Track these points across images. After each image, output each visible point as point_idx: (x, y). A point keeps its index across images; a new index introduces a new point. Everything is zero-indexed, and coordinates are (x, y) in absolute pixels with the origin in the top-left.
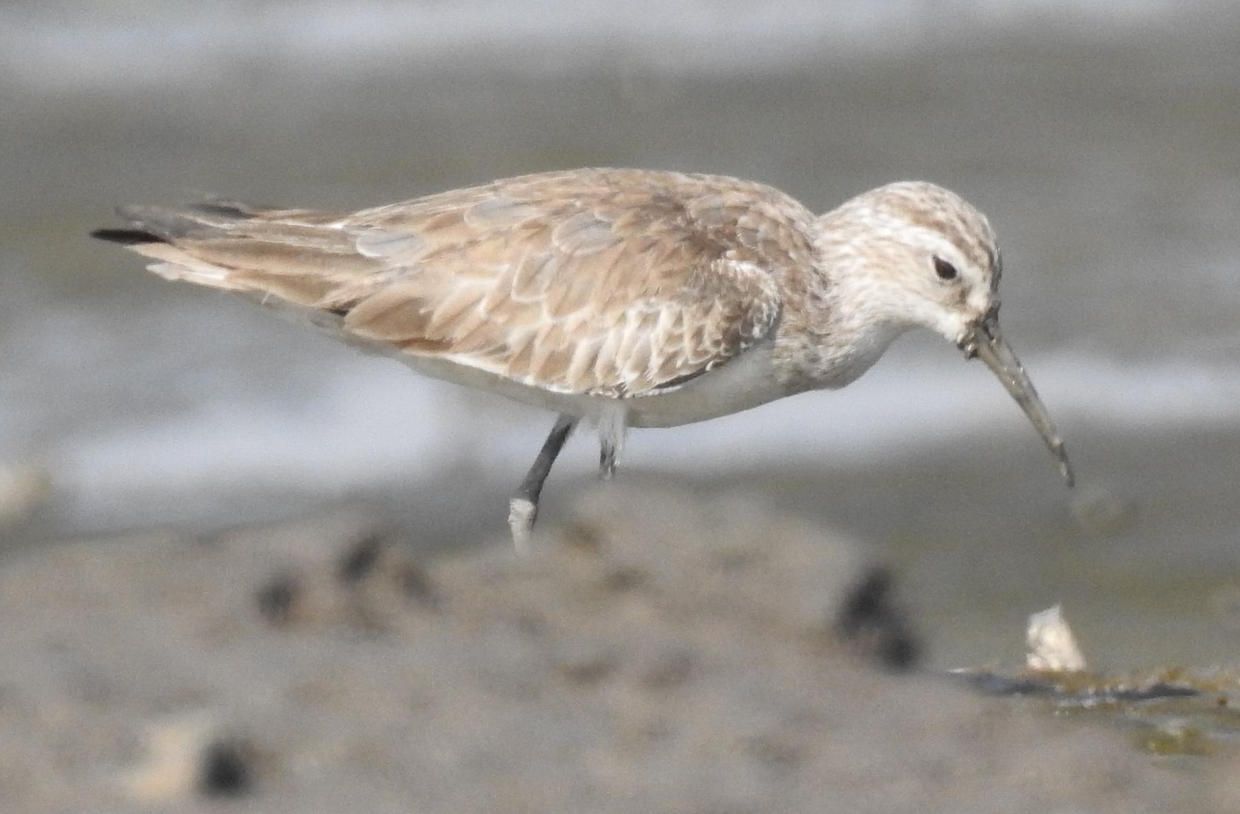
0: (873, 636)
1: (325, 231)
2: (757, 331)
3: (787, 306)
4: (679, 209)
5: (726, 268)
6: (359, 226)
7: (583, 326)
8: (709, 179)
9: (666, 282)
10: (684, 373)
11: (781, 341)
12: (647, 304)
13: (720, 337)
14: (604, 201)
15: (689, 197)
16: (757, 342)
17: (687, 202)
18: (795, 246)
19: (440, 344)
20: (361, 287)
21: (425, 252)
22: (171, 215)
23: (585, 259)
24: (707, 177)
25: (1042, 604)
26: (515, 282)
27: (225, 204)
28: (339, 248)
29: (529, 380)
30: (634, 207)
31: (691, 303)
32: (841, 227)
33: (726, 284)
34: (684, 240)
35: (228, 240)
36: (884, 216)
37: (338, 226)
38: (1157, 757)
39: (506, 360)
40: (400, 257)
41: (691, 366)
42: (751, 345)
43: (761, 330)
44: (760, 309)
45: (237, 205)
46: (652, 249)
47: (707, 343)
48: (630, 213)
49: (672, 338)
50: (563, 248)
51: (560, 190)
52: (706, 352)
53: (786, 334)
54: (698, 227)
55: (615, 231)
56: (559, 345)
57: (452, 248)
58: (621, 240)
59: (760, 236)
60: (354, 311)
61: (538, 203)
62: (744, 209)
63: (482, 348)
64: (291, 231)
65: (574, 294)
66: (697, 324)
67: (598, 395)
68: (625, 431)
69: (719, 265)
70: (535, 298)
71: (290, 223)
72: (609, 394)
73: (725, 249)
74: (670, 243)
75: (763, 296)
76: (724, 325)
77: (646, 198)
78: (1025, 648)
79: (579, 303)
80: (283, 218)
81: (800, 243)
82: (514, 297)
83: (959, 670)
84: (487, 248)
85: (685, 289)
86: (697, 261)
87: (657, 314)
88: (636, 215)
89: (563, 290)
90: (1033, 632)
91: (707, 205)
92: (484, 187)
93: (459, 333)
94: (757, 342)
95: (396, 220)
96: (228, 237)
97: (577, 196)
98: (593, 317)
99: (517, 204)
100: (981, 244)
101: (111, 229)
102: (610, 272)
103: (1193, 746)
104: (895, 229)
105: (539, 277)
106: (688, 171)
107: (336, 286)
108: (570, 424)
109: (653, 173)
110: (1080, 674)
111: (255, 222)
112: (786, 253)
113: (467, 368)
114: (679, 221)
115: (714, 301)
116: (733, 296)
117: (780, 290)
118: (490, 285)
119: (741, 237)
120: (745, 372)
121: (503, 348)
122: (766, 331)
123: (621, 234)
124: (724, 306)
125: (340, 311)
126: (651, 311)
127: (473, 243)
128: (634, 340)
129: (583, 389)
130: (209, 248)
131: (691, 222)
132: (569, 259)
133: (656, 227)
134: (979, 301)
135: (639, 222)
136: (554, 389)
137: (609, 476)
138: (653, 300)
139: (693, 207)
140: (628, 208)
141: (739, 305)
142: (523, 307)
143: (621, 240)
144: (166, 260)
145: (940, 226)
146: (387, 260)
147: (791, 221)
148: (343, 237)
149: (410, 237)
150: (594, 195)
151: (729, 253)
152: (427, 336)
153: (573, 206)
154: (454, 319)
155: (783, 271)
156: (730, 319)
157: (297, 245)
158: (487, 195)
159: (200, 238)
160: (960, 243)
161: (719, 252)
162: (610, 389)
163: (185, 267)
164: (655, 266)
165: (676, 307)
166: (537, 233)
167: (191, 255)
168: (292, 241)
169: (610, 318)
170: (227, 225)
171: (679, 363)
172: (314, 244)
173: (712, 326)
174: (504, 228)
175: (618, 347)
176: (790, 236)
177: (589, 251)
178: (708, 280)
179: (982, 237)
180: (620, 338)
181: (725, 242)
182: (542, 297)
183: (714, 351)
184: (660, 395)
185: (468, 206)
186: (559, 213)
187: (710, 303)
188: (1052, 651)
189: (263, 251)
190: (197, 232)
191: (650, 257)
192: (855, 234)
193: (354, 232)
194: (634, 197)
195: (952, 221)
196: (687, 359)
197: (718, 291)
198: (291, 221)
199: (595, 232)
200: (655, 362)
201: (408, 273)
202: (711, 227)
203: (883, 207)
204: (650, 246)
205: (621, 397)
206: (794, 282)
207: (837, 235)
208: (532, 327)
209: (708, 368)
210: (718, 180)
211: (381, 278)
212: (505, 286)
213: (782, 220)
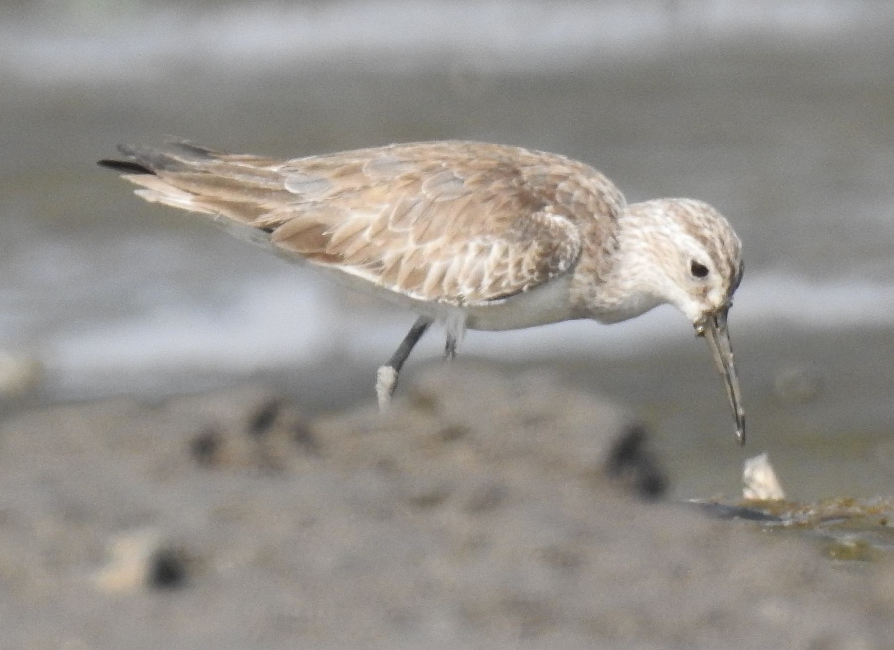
0: (632, 475)
1: (264, 172)
2: (562, 265)
3: (584, 253)
4: (516, 173)
5: (543, 218)
6: (288, 170)
7: (436, 252)
8: (545, 155)
9: (499, 225)
11: (577, 276)
12: (485, 240)
13: (534, 267)
14: (462, 164)
15: (525, 165)
16: (563, 274)
18: (600, 211)
19: (336, 258)
20: (284, 213)
21: (332, 191)
22: (157, 153)
23: (443, 205)
24: (544, 153)
25: (755, 453)
26: (392, 217)
27: (197, 147)
28: (272, 185)
29: (396, 288)
30: (483, 169)
31: (515, 241)
32: (640, 216)
33: (542, 231)
34: (515, 195)
35: (195, 174)
36: (669, 220)
37: (274, 169)
38: (837, 562)
39: (381, 272)
40: (315, 195)
41: (515, 287)
42: (557, 274)
43: (565, 265)
44: (565, 250)
45: (205, 148)
46: (491, 200)
47: (525, 271)
48: (479, 174)
49: (500, 266)
50: (428, 196)
51: (433, 154)
52: (523, 278)
53: (581, 272)
54: (527, 187)
55: (466, 186)
57: (350, 190)
58: (470, 192)
59: (574, 199)
60: (278, 230)
61: (416, 162)
62: (564, 178)
63: (364, 263)
64: (240, 171)
65: (433, 228)
66: (519, 257)
67: (444, 303)
68: (464, 332)
69: (538, 216)
71: (241, 165)
72: (452, 302)
73: (545, 205)
74: (505, 198)
75: (568, 240)
76: (538, 258)
77: (493, 163)
78: (741, 484)
79: (436, 235)
81: (604, 209)
82: (390, 228)
84: (377, 191)
85: (512, 231)
86: (522, 211)
88: (483, 176)
89: (426, 224)
90: (747, 472)
91: (536, 172)
92: (381, 148)
93: (349, 251)
94: (563, 274)
95: (315, 167)
96: (195, 171)
97: (444, 159)
98: (444, 245)
99: (401, 163)
102: (458, 216)
103: (862, 554)
105: (409, 215)
106: (530, 147)
107: (267, 211)
108: (427, 323)
109: (504, 147)
110: (781, 502)
111: (216, 162)
112: (591, 215)
113: (354, 277)
114: (514, 182)
117: (582, 238)
118: (374, 218)
119: (558, 198)
120: (550, 295)
121: (380, 264)
122: (569, 265)
123: (471, 188)
124: (540, 245)
126: (485, 245)
127: (365, 188)
128: (472, 265)
129: (434, 297)
130: (180, 178)
131: (522, 183)
132: (432, 203)
133: (496, 185)
134: (716, 298)
135: (484, 181)
136: (414, 296)
137: (449, 358)
138: (488, 237)
139: (526, 173)
140: (480, 170)
142: (396, 236)
143: (470, 192)
144: (149, 187)
145: (704, 240)
146: (304, 196)
147: (601, 194)
148: (276, 177)
149: (322, 180)
150: (456, 159)
151: (547, 208)
153: (440, 166)
154: (346, 240)
155: (588, 227)
156: (544, 255)
157: (242, 181)
158: (382, 154)
159: (174, 171)
160: (714, 256)
161: (539, 206)
162: (453, 299)
163: (162, 193)
164: (493, 212)
165: (504, 243)
166: (412, 183)
167: (167, 183)
168: (239, 178)
169: (457, 247)
170: (195, 163)
171: (504, 284)
172: (254, 181)
173: (529, 259)
174: (389, 178)
176: (598, 204)
177: (447, 198)
178: (528, 226)
180: (462, 263)
181: (545, 199)
182: (411, 229)
183: (529, 277)
185: (367, 161)
186: (430, 170)
187: (529, 243)
188: (760, 485)
189: (218, 184)
190: (175, 167)
191: (489, 206)
192: (646, 224)
193: (283, 175)
194: (484, 163)
196: (509, 282)
197: (536, 234)
198: (241, 163)
199: (452, 185)
200: (487, 282)
201: (318, 206)
202: (537, 188)
203: (672, 213)
204: (489, 199)
205: (461, 305)
206: (594, 236)
207: (635, 221)
209: (525, 288)
210: (551, 157)
211: (298, 208)
212: (384, 220)
213: (594, 191)
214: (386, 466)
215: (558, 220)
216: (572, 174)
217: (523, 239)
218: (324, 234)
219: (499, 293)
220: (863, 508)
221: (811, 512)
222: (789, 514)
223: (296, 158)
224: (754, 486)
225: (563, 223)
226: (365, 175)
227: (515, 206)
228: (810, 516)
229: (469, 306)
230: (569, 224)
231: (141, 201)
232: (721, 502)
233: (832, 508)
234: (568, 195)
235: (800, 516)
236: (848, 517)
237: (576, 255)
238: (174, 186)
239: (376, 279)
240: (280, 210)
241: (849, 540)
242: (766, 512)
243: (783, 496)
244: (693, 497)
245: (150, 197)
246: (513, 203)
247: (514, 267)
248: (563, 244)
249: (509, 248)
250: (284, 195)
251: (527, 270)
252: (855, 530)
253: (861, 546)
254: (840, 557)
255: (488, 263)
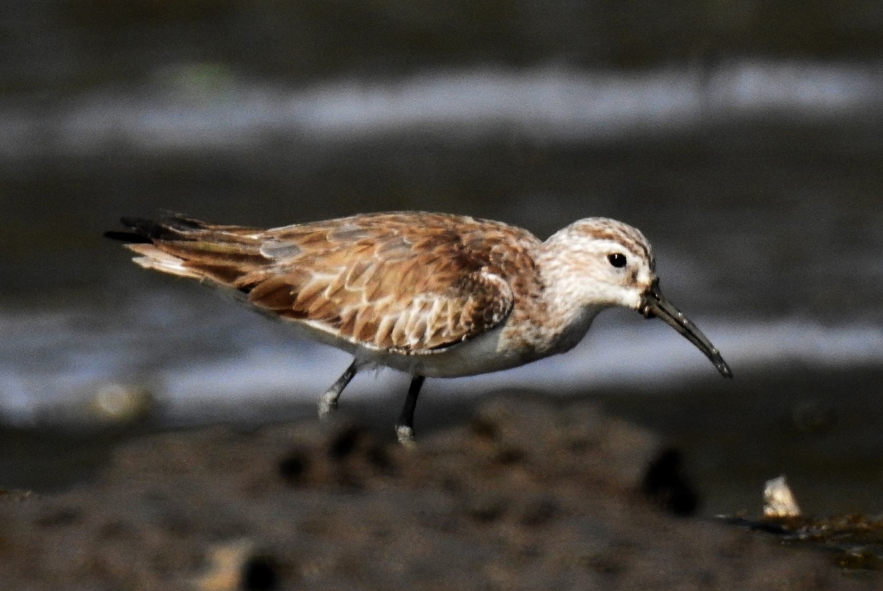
2: (495, 318)
4: (457, 239)
7: (386, 307)
9: (439, 284)
10: (448, 341)
12: (427, 297)
13: (471, 320)
15: (465, 232)
17: (464, 235)
19: (304, 315)
23: (392, 267)
25: (773, 475)
26: (348, 278)
28: (249, 249)
29: (353, 340)
34: (453, 258)
36: (575, 238)
37: (255, 237)
38: (846, 570)
39: (337, 327)
41: (452, 337)
43: (499, 317)
44: (497, 304)
47: (462, 323)
49: (439, 318)
51: (389, 222)
52: (461, 329)
55: (413, 251)
56: (371, 319)
60: (254, 290)
62: (496, 241)
67: (394, 351)
70: (359, 289)
72: (401, 351)
73: (481, 266)
75: (501, 296)
76: (473, 312)
77: (439, 231)
78: (764, 502)
80: (222, 230)
81: (528, 262)
82: (346, 287)
83: (721, 516)
85: (451, 288)
87: (432, 303)
89: (377, 284)
90: (768, 492)
93: (312, 308)
100: (637, 243)
101: (513, 369)
104: (583, 244)
107: (243, 274)
110: (797, 519)
114: (455, 247)
115: (467, 299)
116: (480, 294)
121: (338, 319)
122: (502, 317)
123: (416, 252)
125: (245, 289)
128: (417, 318)
129: (384, 348)
131: (462, 248)
132: (382, 265)
136: (368, 346)
138: (430, 294)
139: (465, 239)
140: (427, 236)
141: (484, 300)
143: (415, 256)
145: (610, 237)
147: (525, 251)
148: (257, 244)
149: (293, 247)
152: (294, 308)
154: (313, 296)
155: (514, 279)
156: (478, 309)
158: (348, 224)
160: (624, 243)
161: (478, 268)
162: (401, 348)
164: (435, 272)
165: (444, 299)
167: (162, 250)
171: (444, 334)
175: (407, 323)
176: (523, 260)
179: (637, 239)
180: (408, 316)
184: (432, 354)
185: (331, 230)
191: (431, 268)
192: (559, 252)
195: (617, 233)
196: (449, 334)
199: (401, 250)
200: (429, 333)
202: (474, 252)
205: (408, 354)
207: (549, 255)
208: (356, 307)
209: (463, 338)
211: (269, 271)
213: (520, 250)
214: (450, 485)
215: (493, 278)
216: (505, 238)
217: (460, 295)
218: (292, 293)
219: (441, 342)
220: (869, 523)
221: (824, 527)
222: (804, 529)
223: (274, 227)
224: (774, 504)
225: (496, 280)
226: (328, 241)
227: (454, 266)
228: (823, 531)
229: (416, 354)
230: (503, 282)
231: (138, 267)
232: (744, 518)
233: (842, 523)
234: (499, 255)
235: (815, 531)
236: (857, 532)
237: (508, 308)
238: (167, 253)
239: (336, 332)
240: (254, 273)
241: (856, 552)
242: (785, 527)
243: (799, 513)
244: (719, 513)
245: (145, 264)
246: (453, 265)
247: (452, 320)
248: (496, 299)
249: (448, 303)
250: (258, 260)
251: (464, 323)
252: (860, 543)
253: (867, 556)
254: (849, 566)
255: (429, 316)
